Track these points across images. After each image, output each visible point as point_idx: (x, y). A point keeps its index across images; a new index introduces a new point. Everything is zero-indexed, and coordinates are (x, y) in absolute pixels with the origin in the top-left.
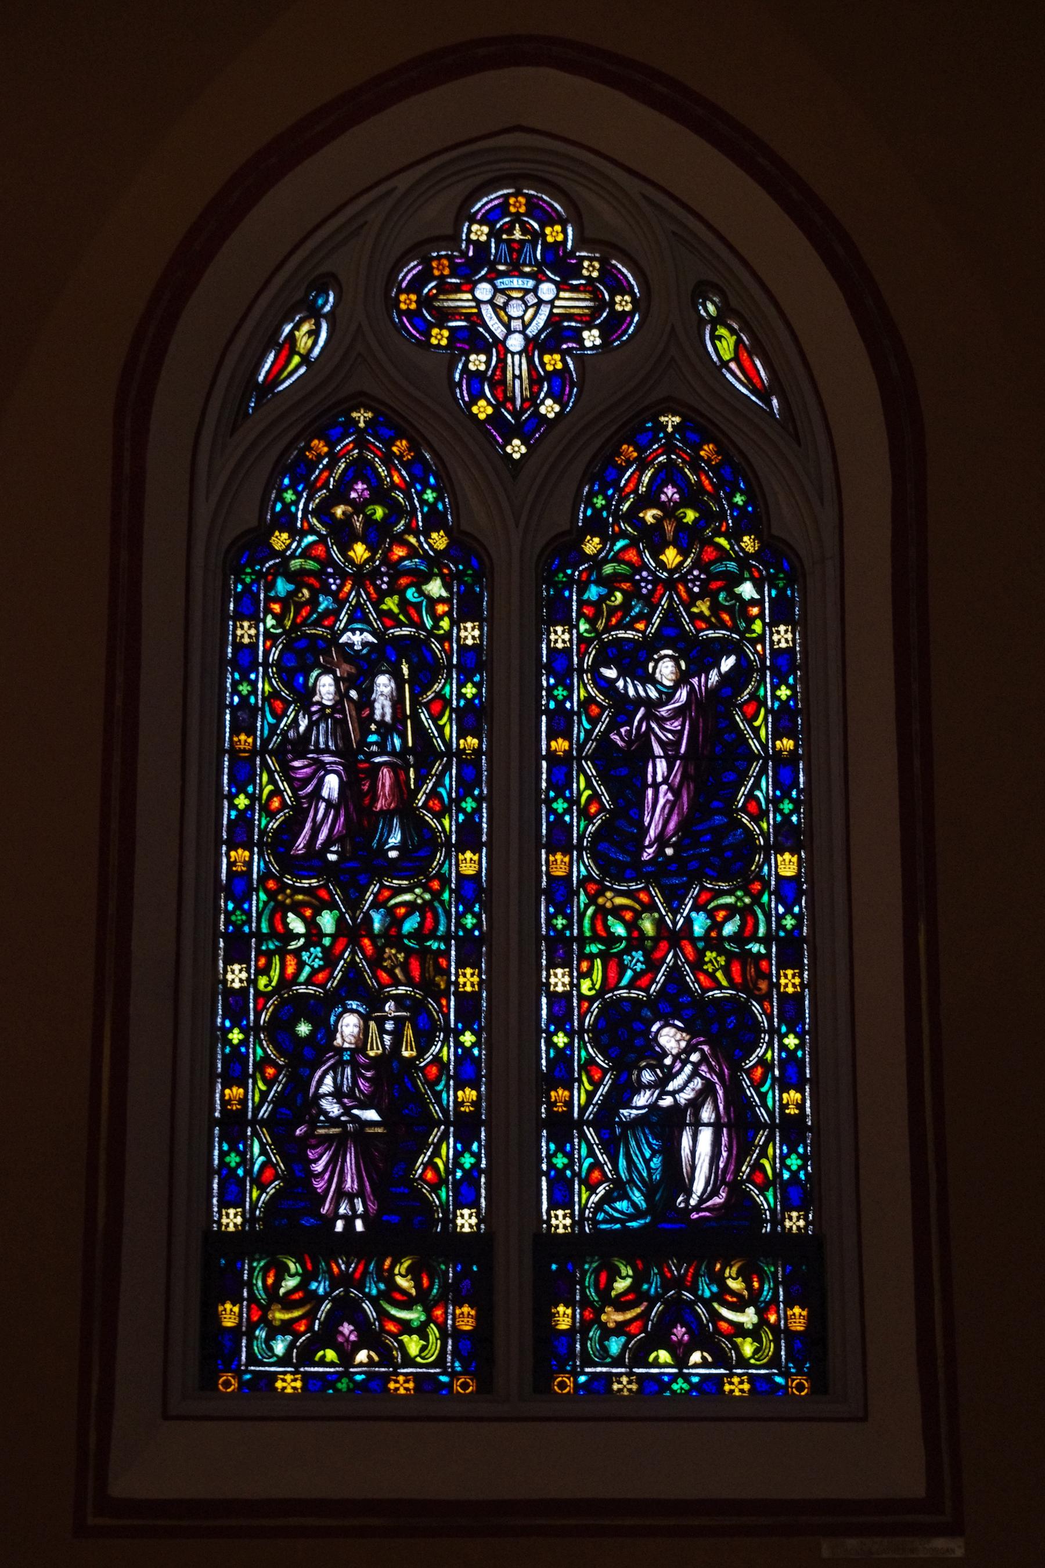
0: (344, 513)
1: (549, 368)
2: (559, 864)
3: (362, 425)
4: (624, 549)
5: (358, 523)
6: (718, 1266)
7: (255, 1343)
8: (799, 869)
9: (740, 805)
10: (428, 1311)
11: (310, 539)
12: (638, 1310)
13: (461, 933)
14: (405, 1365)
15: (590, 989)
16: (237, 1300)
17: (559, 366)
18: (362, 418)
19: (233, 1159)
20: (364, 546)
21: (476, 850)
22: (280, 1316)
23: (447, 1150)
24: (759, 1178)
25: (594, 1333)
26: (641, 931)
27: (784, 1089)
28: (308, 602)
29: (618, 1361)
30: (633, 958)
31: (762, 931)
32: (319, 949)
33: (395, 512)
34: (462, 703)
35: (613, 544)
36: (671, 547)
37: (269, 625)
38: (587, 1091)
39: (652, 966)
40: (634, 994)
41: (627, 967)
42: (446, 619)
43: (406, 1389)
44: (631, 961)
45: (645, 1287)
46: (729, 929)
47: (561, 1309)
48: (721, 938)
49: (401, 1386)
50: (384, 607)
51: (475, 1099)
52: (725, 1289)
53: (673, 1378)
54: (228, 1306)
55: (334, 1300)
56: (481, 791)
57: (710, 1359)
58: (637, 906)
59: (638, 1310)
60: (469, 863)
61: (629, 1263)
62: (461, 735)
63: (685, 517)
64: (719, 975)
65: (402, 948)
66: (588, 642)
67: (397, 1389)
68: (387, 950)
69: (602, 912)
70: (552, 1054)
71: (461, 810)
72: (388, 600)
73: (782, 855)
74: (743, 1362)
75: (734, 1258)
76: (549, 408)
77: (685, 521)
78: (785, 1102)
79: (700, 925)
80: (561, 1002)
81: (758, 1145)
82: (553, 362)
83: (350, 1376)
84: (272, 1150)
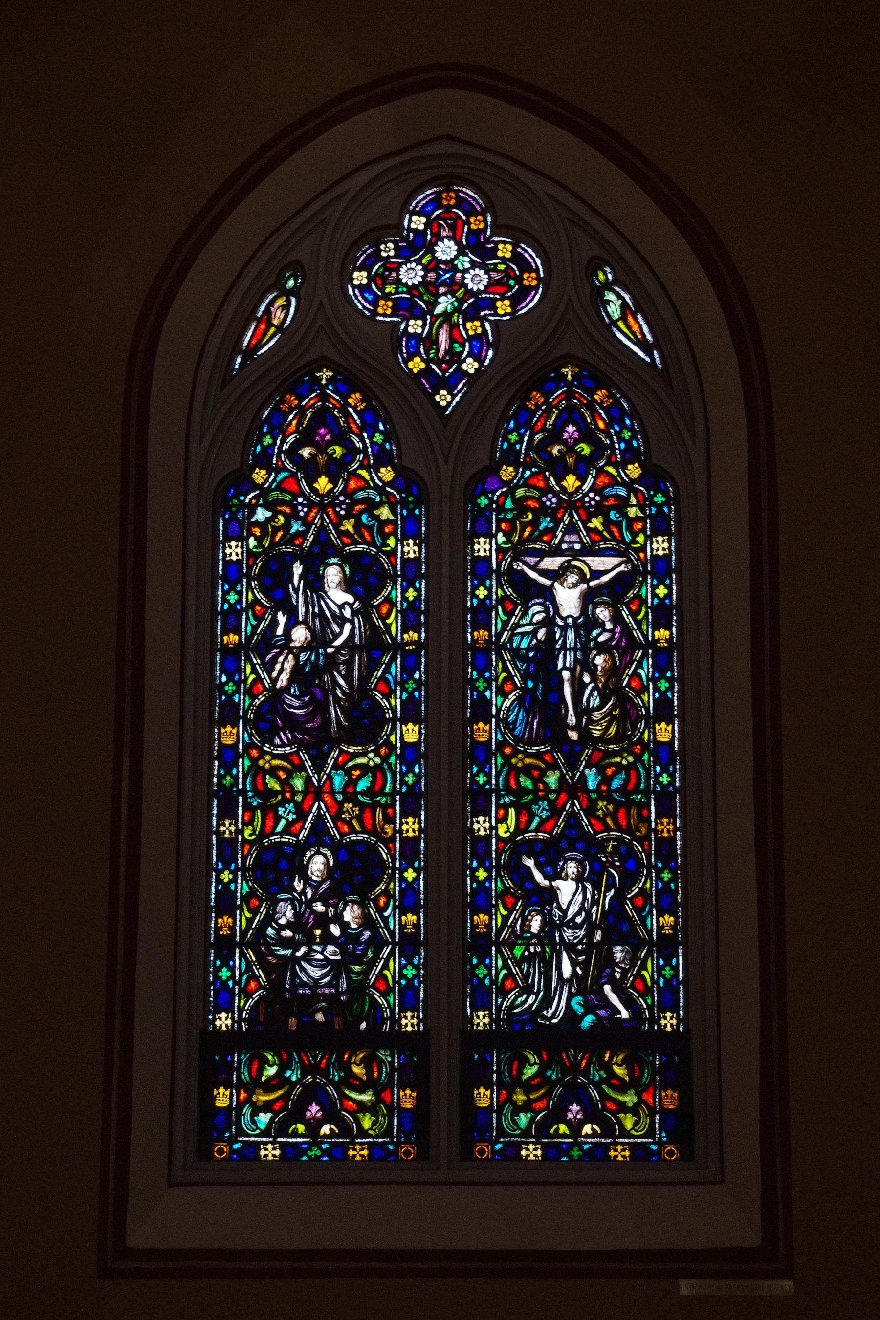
0: (559, 451)
1: (471, 333)
2: (229, 735)
3: (569, 378)
6: (607, 1055)
8: (420, 737)
10: (638, 1094)
11: (283, 475)
12: (280, 1092)
13: (658, 788)
14: (622, 1136)
15: (506, 832)
17: (479, 331)
18: (570, 373)
20: (574, 478)
21: (669, 722)
22: (263, 1098)
23: (394, 965)
25: (247, 1110)
30: (286, 809)
31: (388, 789)
33: (599, 449)
34: (226, 606)
37: (251, 546)
39: (302, 815)
40: (541, 835)
41: (281, 817)
45: (549, 1073)
46: (363, 785)
48: (610, 791)
49: (620, 1153)
50: (342, 528)
52: (612, 1074)
55: (304, 1086)
56: (673, 674)
58: (543, 766)
59: (280, 1092)
60: (664, 732)
61: (537, 1053)
62: (405, 631)
63: (334, 453)
64: (354, 822)
66: (257, 555)
67: (616, 1156)
69: (515, 772)
72: (594, 519)
73: (225, 728)
76: (470, 366)
77: (334, 456)
78: (661, 924)
79: (339, 781)
80: (228, 848)
82: (473, 327)
83: (580, 1145)
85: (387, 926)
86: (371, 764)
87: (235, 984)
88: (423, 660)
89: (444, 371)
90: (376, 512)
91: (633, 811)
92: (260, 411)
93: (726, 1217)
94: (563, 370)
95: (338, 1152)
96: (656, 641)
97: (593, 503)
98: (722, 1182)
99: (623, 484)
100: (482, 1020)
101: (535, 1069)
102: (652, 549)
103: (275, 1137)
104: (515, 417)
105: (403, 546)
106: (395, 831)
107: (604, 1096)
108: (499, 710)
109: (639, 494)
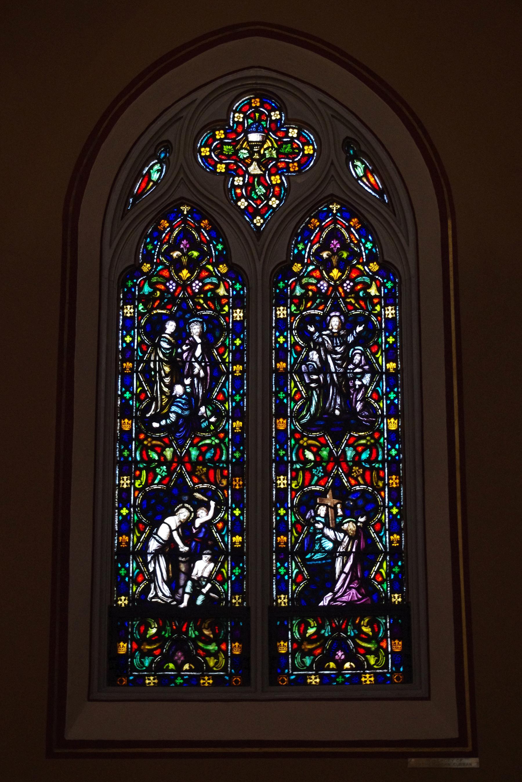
1: (274, 183)
3: (185, 213)
4: (312, 270)
5: (184, 260)
7: (135, 660)
9: (369, 395)
10: (218, 645)
11: (160, 267)
16: (286, 640)
17: (279, 181)
19: (282, 571)
24: (219, 578)
26: (165, 457)
27: (233, 535)
28: (158, 298)
29: (310, 668)
30: (317, 470)
31: (380, 458)
32: (321, 467)
35: (307, 269)
36: (185, 270)
37: (293, 310)
38: (295, 537)
42: (227, 306)
43: (370, 681)
44: (356, 473)
46: (365, 456)
47: (122, 644)
49: (368, 679)
51: (241, 541)
53: (337, 676)
54: (282, 643)
57: (193, 667)
64: (359, 479)
65: (361, 467)
66: (144, 314)
68: (354, 468)
70: (121, 518)
71: (388, 398)
73: (390, 420)
74: (370, 667)
75: (365, 616)
76: (274, 202)
79: (350, 453)
80: (282, 493)
81: (379, 561)
84: (301, 565)
85: (223, 541)
86: (213, 443)
87: (289, 578)
88: (245, 382)
89: (258, 205)
90: (368, 291)
91: (218, 471)
92: (147, 228)
93: (437, 718)
94: (182, 208)
95: (356, 679)
96: (387, 370)
97: (349, 287)
98: (428, 698)
99: (368, 275)
100: (123, 601)
101: (314, 629)
102: (385, 314)
103: (155, 672)
104: (151, 236)
105: (385, 311)
106: (384, 484)
107: (357, 645)
108: (292, 411)
109: (378, 281)
